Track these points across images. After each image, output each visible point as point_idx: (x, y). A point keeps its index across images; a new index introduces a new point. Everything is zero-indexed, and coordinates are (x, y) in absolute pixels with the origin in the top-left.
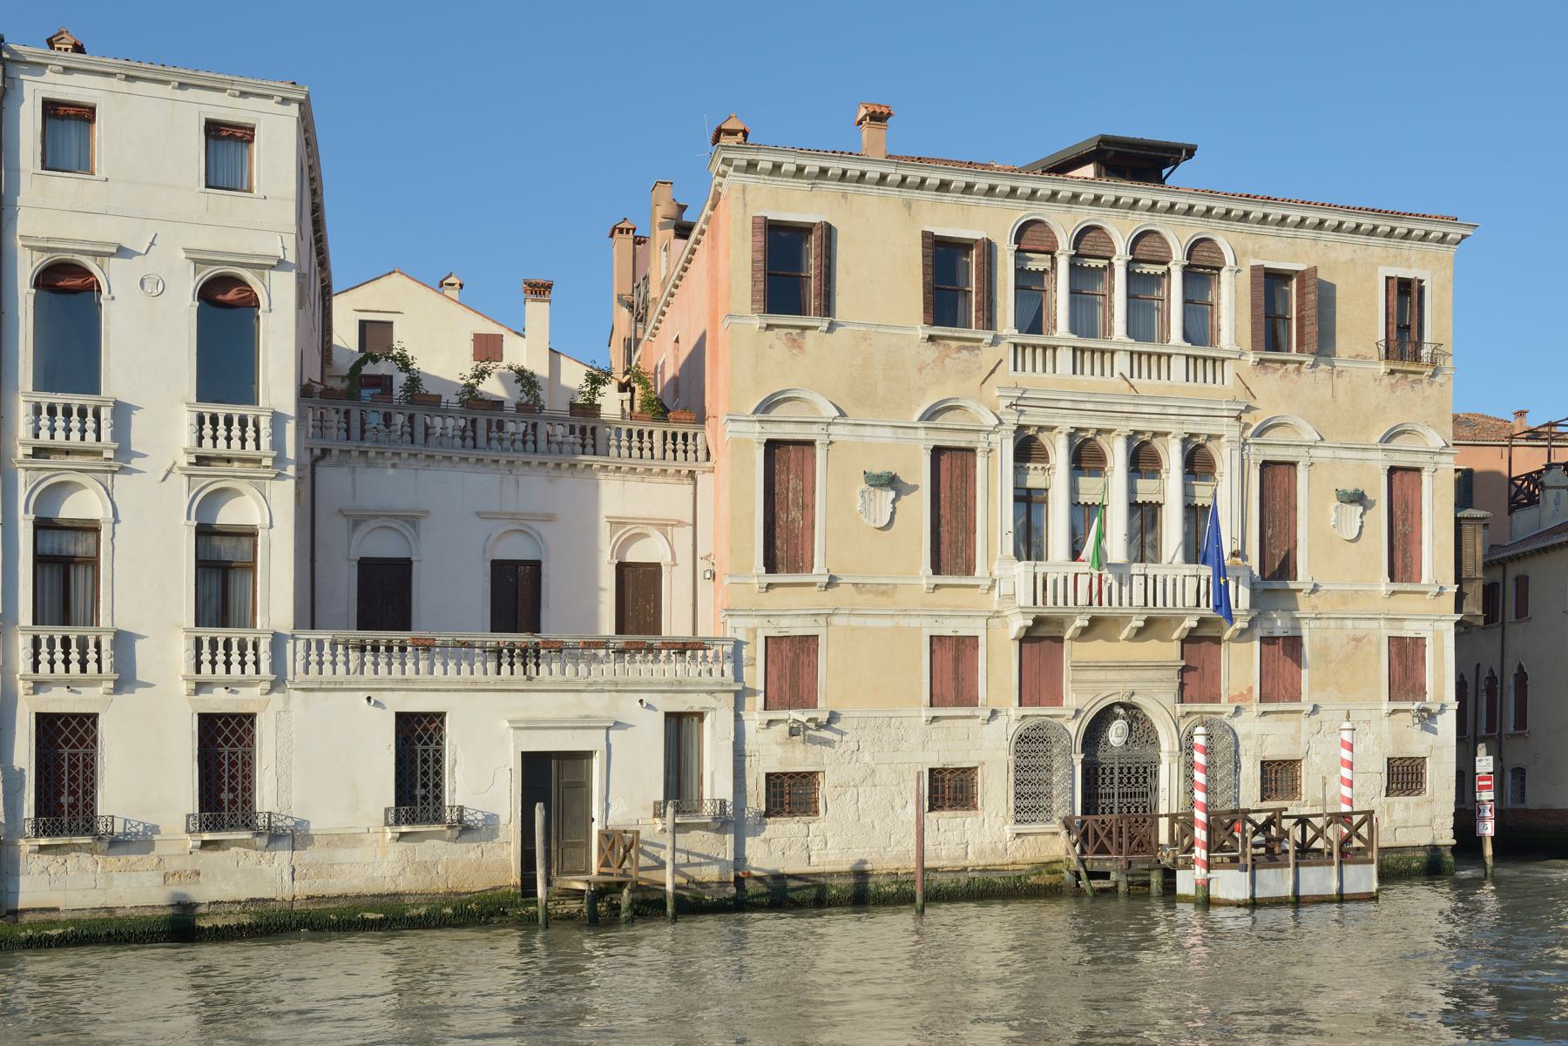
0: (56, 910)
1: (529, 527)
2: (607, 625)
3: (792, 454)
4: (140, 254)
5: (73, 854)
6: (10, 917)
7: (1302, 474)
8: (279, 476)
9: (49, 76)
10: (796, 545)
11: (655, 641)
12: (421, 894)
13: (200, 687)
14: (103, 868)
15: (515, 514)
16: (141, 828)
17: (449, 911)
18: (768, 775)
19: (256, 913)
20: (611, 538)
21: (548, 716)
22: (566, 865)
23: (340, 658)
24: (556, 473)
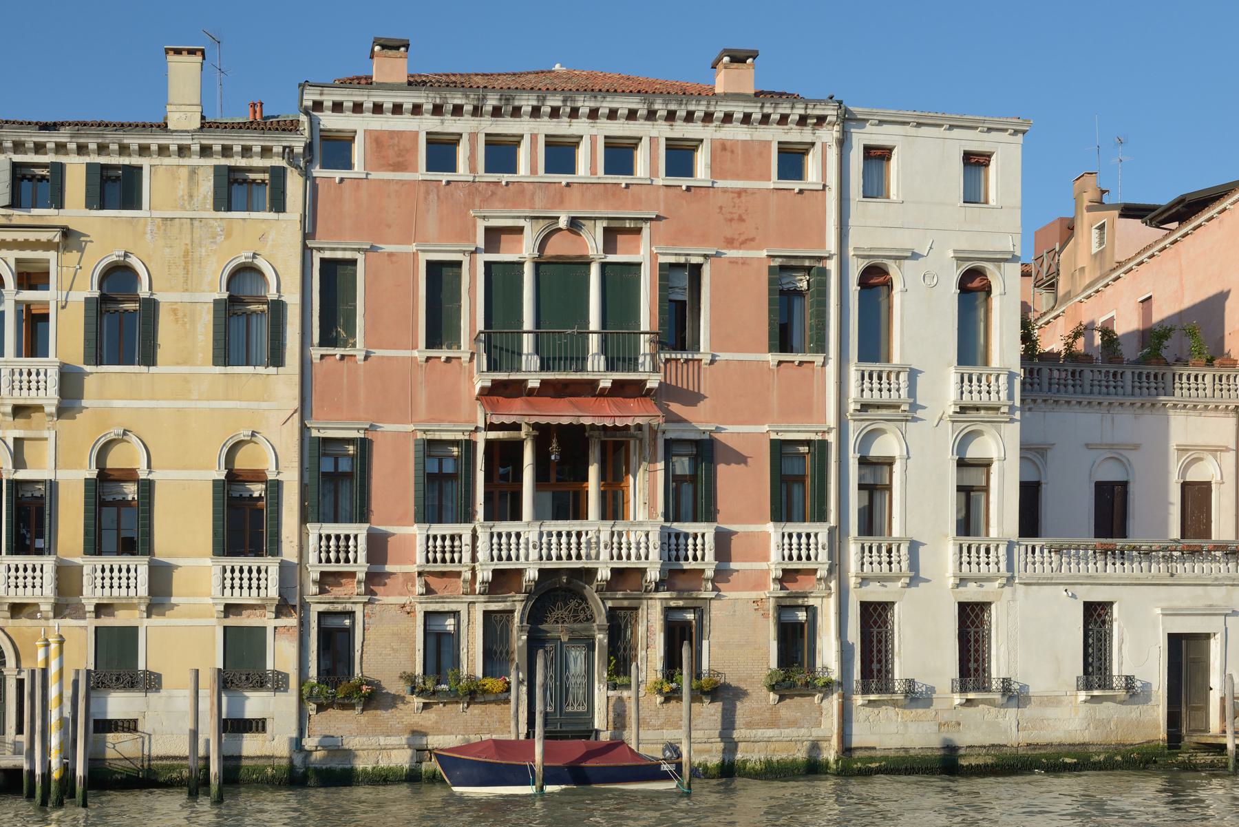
0: (874, 748)
1: (1121, 455)
2: (1175, 532)
4: (923, 256)
5: (884, 707)
6: (847, 753)
8: (1012, 421)
9: (868, 128)
11: (1206, 544)
12: (1101, 745)
13: (963, 581)
14: (902, 718)
15: (1113, 445)
16: (924, 689)
17: (1119, 758)
19: (995, 755)
20: (1178, 461)
21: (1183, 605)
22: (1191, 724)
23: (1047, 559)
24: (1140, 411)
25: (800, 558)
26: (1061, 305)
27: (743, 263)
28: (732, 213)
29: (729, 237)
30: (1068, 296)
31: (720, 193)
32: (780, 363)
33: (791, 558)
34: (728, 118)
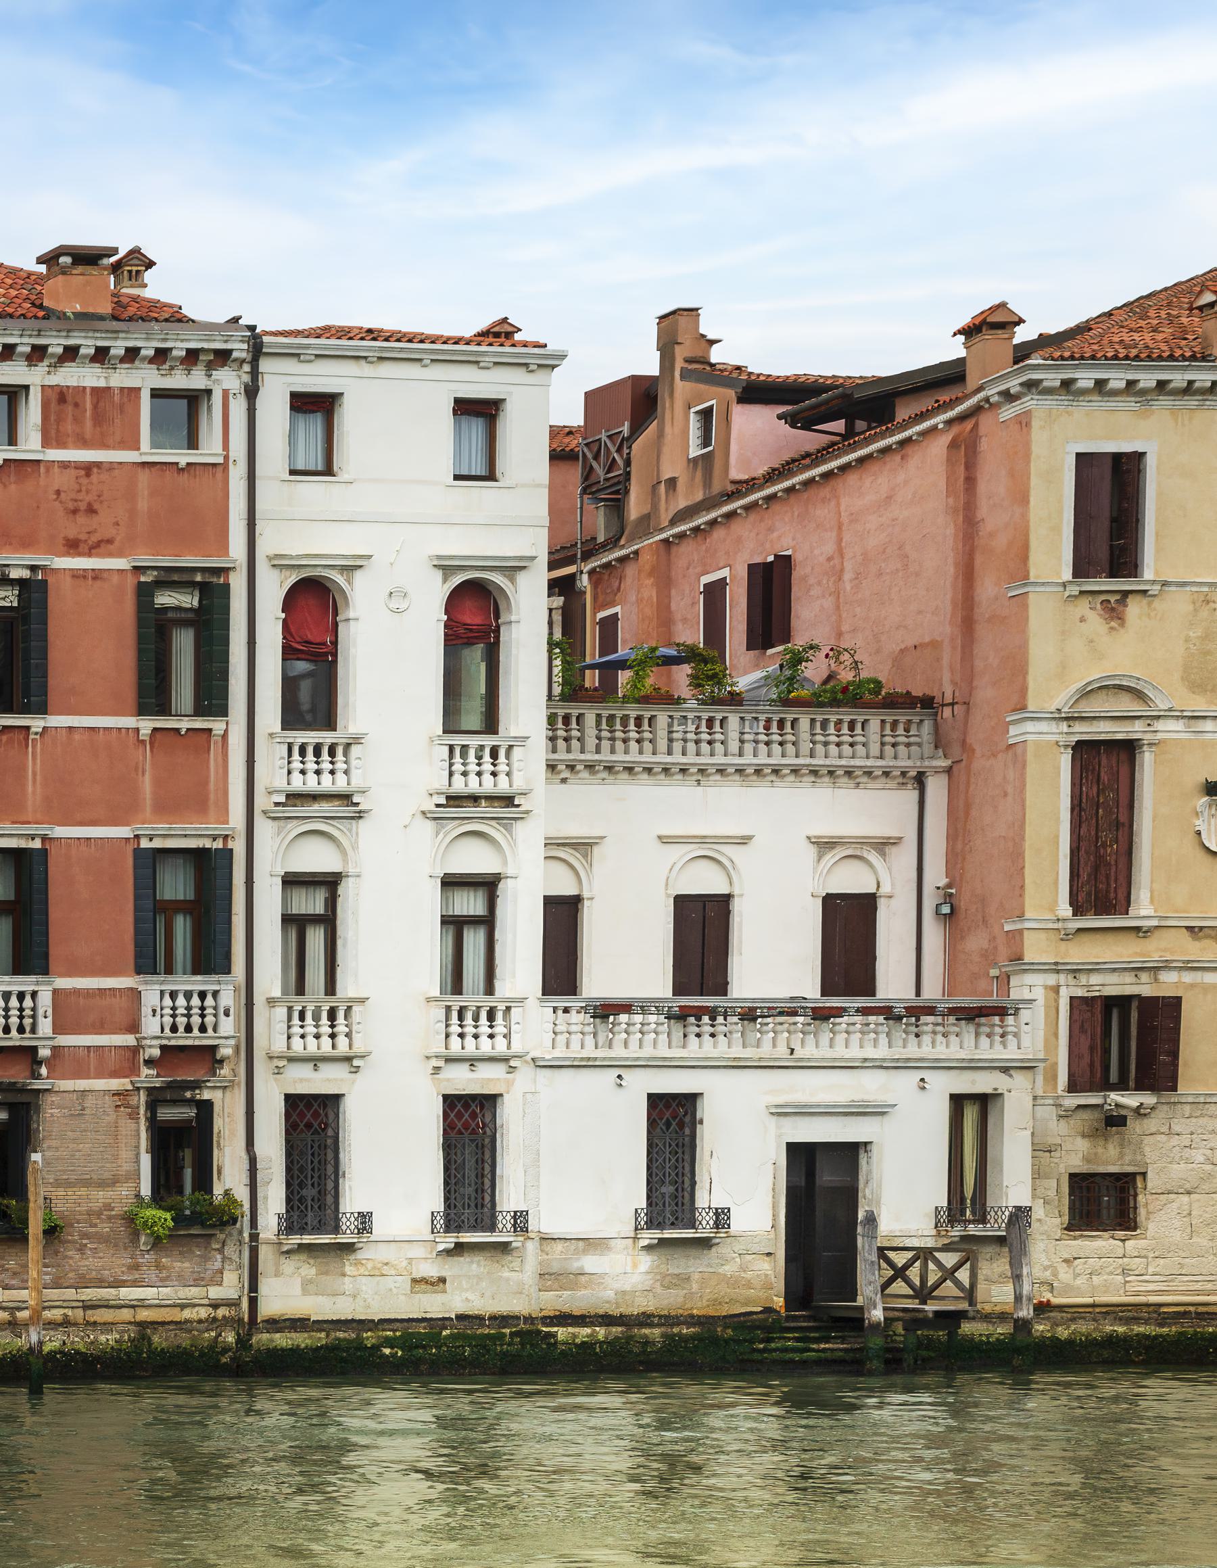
3: (1104, 761)
7: (1147, 760)
10: (1108, 877)
18: (1072, 1176)
25: (189, 1029)
26: (631, 540)
27: (95, 578)
28: (76, 501)
29: (71, 537)
30: (646, 524)
31: (56, 469)
32: (155, 730)
33: (174, 1029)
34: (71, 353)
